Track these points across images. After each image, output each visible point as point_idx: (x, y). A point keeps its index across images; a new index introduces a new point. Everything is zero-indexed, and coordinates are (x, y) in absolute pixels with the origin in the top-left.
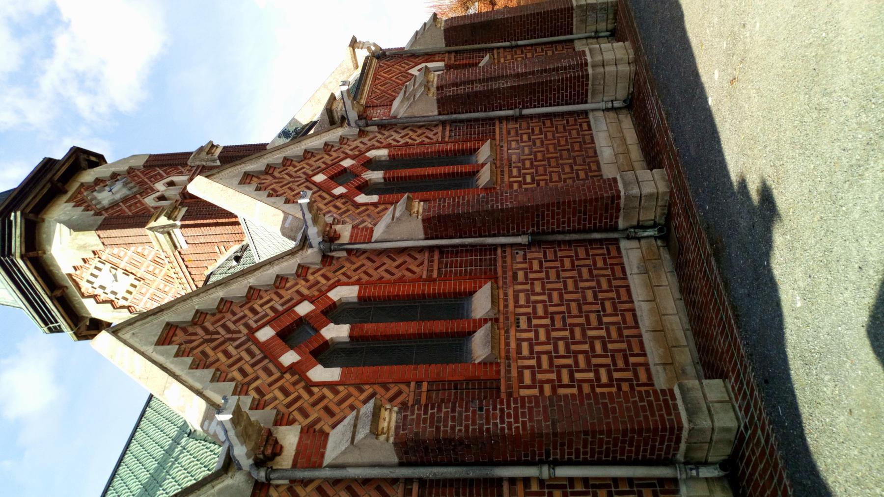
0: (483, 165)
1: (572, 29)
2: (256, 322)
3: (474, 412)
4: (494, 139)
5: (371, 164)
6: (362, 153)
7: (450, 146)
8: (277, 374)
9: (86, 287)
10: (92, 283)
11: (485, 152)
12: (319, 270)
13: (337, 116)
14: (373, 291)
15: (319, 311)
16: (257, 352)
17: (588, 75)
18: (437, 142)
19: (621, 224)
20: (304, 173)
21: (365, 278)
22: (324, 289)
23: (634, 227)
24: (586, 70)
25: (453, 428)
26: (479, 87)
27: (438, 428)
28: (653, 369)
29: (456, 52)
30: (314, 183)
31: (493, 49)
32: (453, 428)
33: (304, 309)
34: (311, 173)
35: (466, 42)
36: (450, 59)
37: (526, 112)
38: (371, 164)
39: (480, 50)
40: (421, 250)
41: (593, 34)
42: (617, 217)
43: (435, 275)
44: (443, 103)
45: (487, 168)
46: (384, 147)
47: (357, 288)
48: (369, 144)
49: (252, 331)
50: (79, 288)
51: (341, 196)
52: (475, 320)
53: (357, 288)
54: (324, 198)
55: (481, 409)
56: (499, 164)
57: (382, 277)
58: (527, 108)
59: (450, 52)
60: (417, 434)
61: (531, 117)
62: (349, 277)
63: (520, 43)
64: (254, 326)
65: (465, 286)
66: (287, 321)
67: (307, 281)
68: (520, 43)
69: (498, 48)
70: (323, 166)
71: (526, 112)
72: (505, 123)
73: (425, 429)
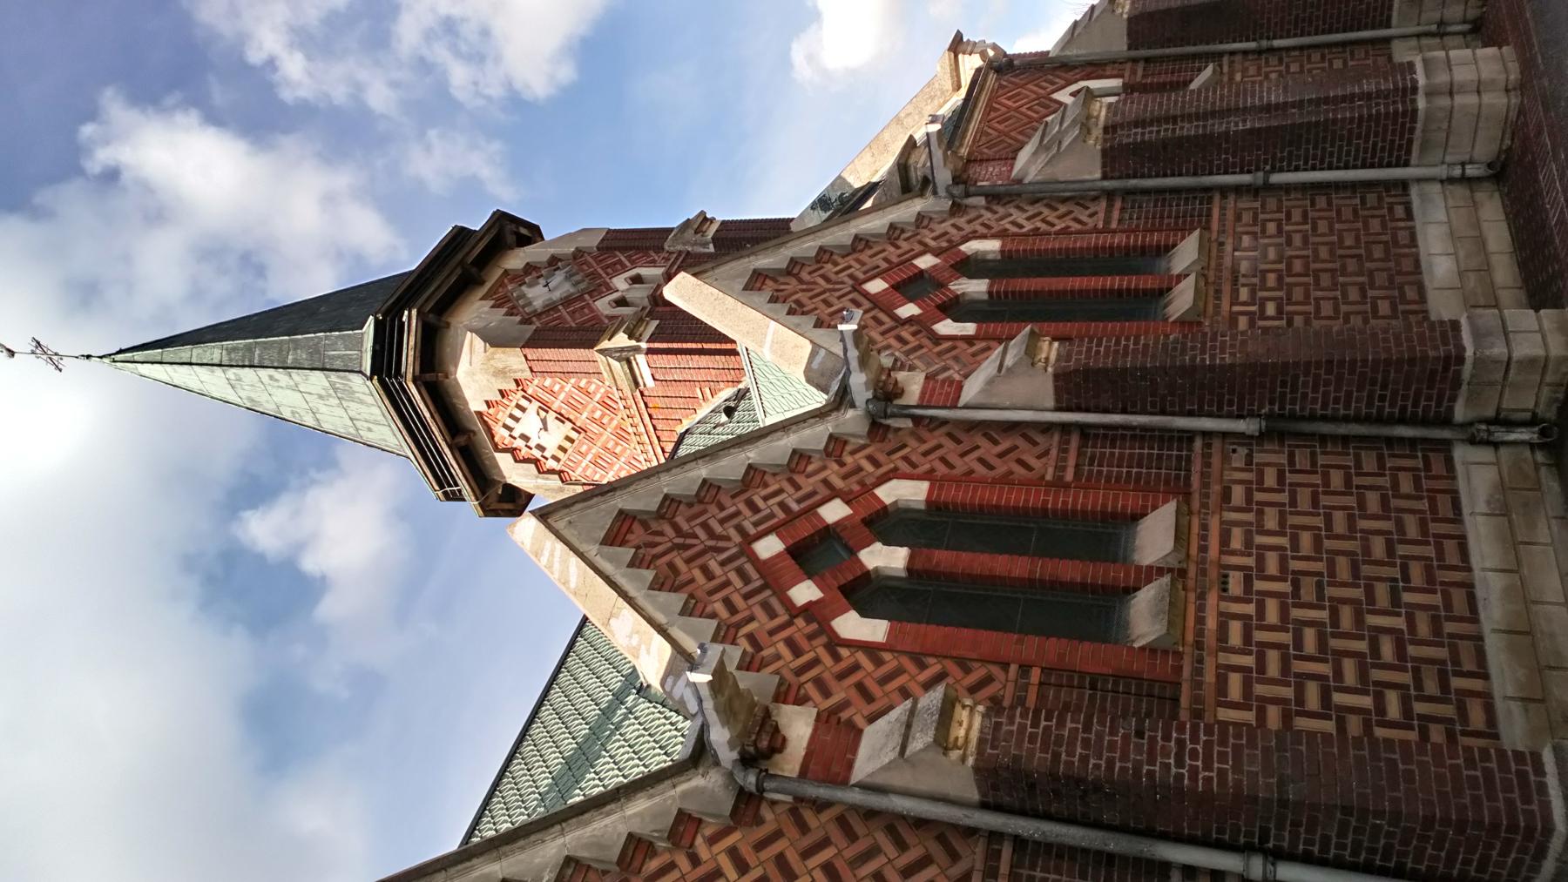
0: (1181, 277)
1: (1389, 18)
2: (756, 524)
3: (1126, 737)
4: (1207, 228)
5: (971, 267)
6: (953, 245)
7: (1120, 239)
8: (783, 618)
9: (501, 434)
10: (510, 429)
11: (1187, 253)
12: (863, 447)
13: (915, 176)
14: (952, 494)
15: (858, 518)
16: (754, 575)
17: (1415, 111)
18: (1095, 230)
19: (1460, 413)
20: (851, 276)
21: (942, 469)
22: (869, 481)
23: (1489, 422)
24: (1414, 101)
25: (1084, 759)
26: (1188, 129)
27: (1056, 756)
28: (1500, 705)
29: (1147, 60)
30: (866, 295)
31: (1221, 54)
32: (1084, 759)
33: (834, 512)
34: (861, 276)
35: (1169, 42)
36: (1134, 72)
37: (1276, 178)
38: (971, 267)
39: (1195, 56)
40: (1046, 428)
41: (1434, 28)
42: (1453, 399)
43: (1069, 476)
44: (1113, 158)
45: (1190, 282)
46: (994, 236)
47: (925, 485)
48: (968, 228)
49: (749, 540)
50: (492, 436)
51: (911, 320)
52: (1139, 568)
53: (925, 485)
54: (881, 323)
55: (1140, 734)
56: (1210, 276)
57: (972, 472)
58: (1281, 170)
59: (1135, 60)
60: (1017, 759)
61: (1287, 188)
62: (914, 466)
63: (1277, 43)
64: (752, 531)
65: (1127, 501)
66: (804, 530)
67: (842, 464)
68: (1277, 43)
69: (1232, 53)
70: (884, 265)
71: (1276, 178)
72: (1231, 198)
73: (1031, 753)
